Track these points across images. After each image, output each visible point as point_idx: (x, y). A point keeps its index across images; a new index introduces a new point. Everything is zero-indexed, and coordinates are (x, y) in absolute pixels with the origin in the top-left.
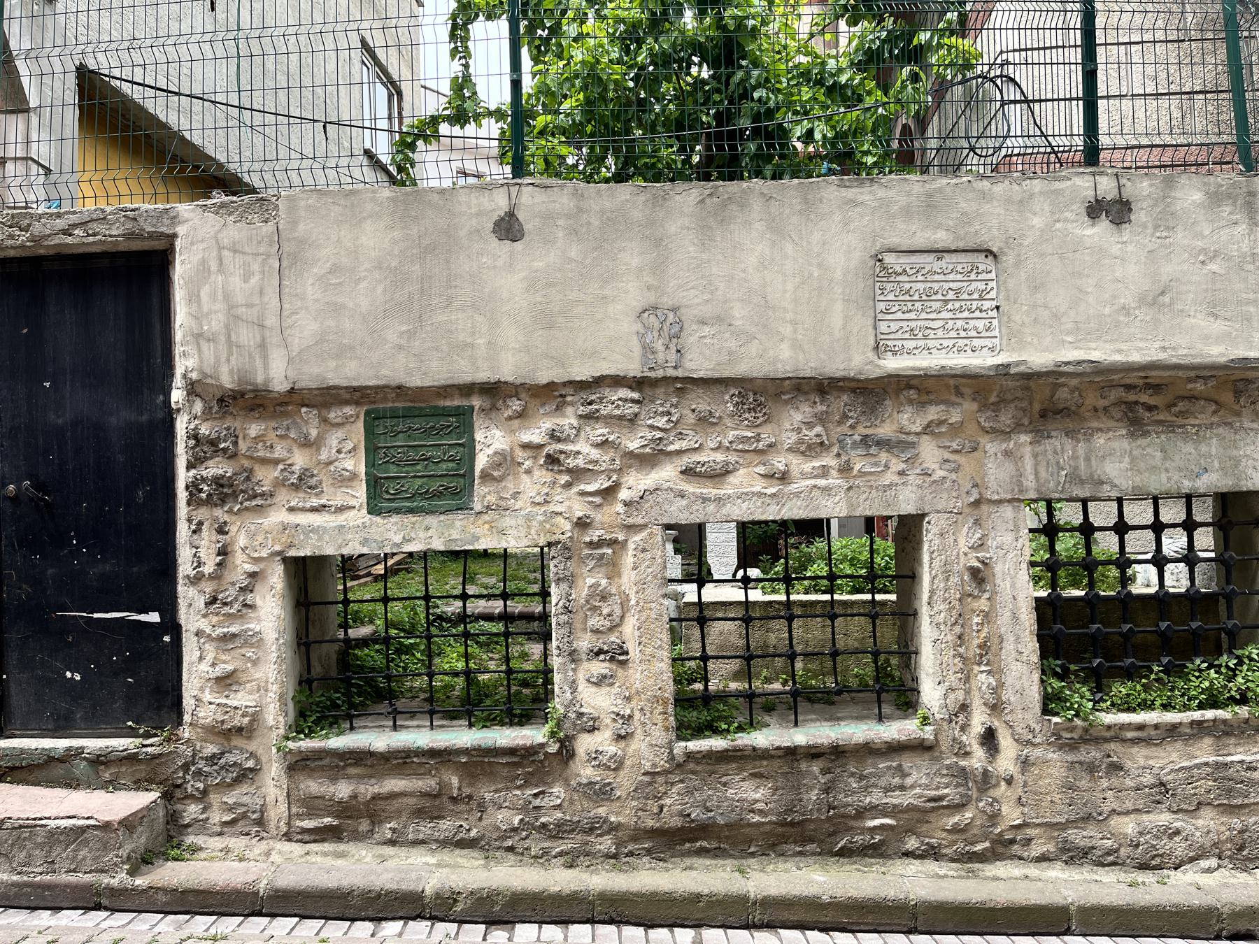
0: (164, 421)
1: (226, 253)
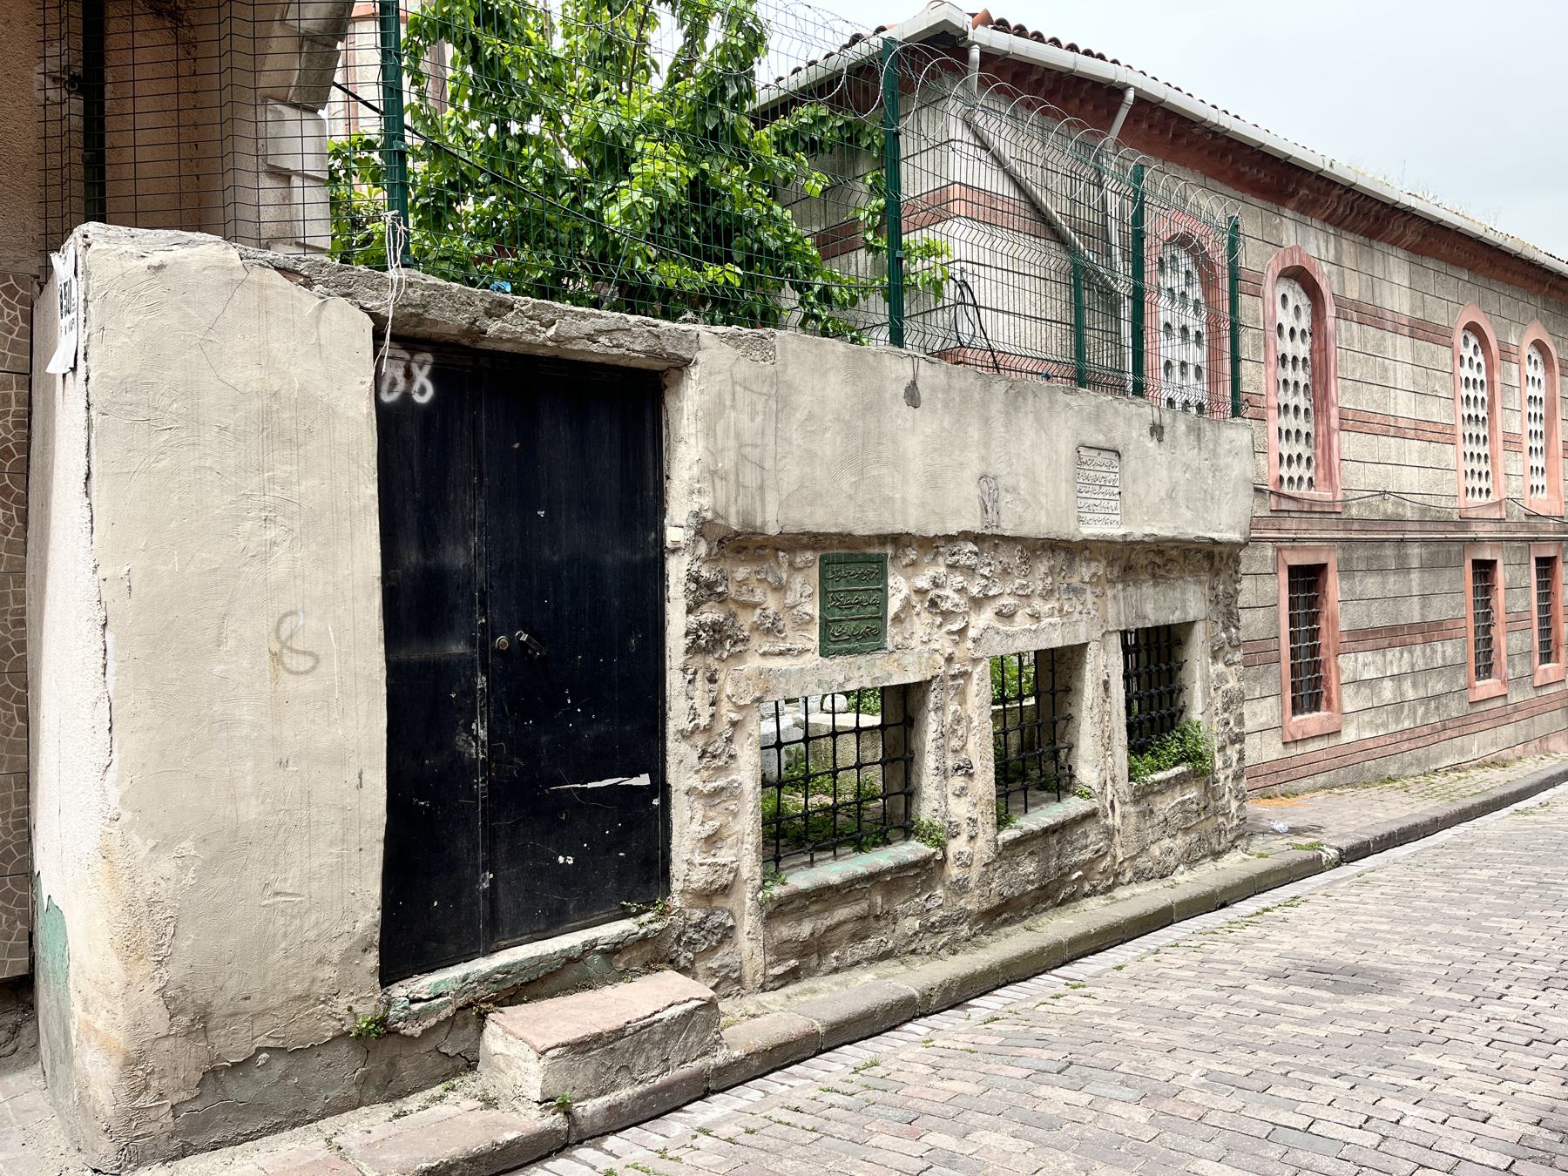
0: (655, 559)
1: (738, 388)
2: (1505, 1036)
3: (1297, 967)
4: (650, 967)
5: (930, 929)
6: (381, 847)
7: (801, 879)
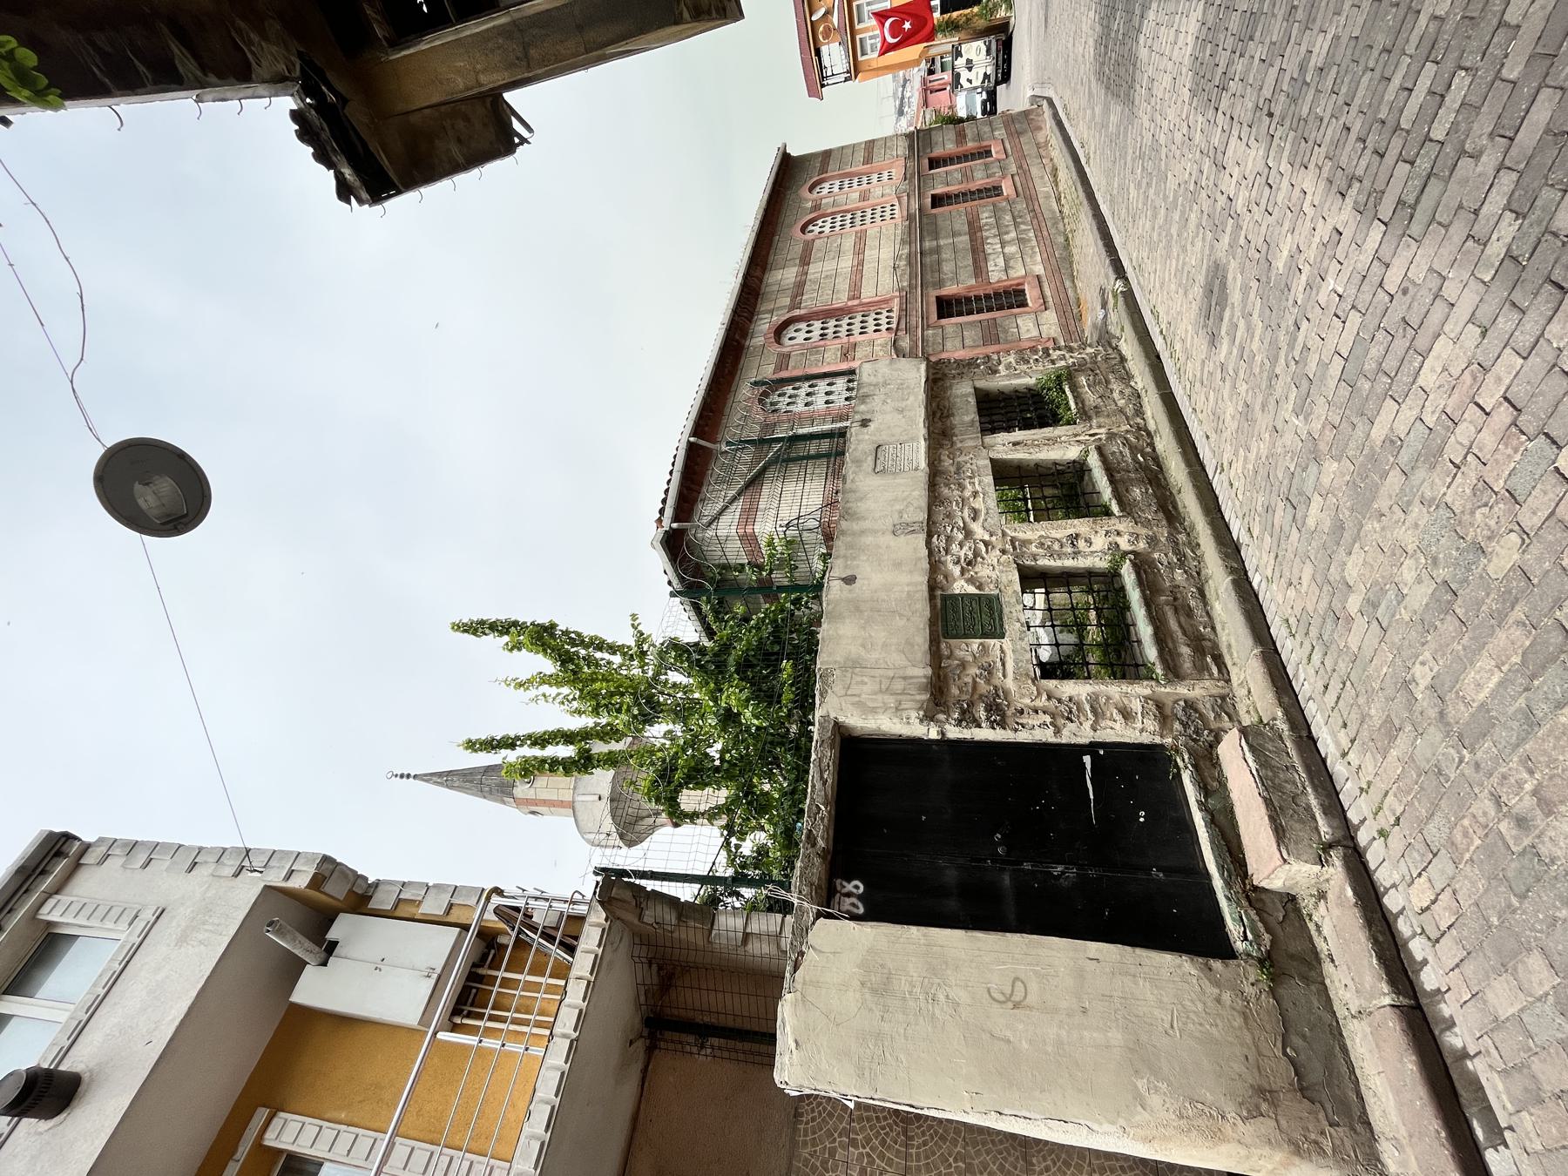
2: (1263, 202)
3: (1206, 326)
4: (1215, 763)
5: (1182, 562)
6: (1138, 951)
7: (1151, 653)
